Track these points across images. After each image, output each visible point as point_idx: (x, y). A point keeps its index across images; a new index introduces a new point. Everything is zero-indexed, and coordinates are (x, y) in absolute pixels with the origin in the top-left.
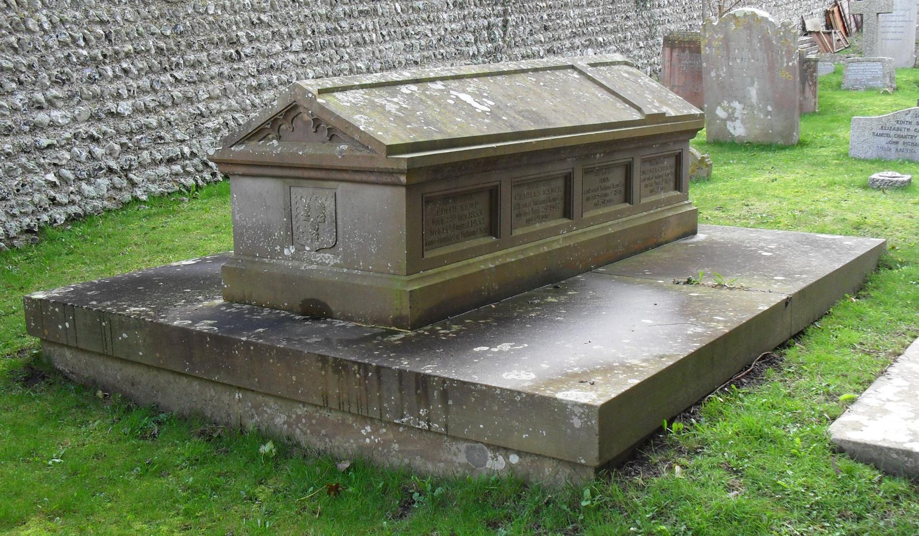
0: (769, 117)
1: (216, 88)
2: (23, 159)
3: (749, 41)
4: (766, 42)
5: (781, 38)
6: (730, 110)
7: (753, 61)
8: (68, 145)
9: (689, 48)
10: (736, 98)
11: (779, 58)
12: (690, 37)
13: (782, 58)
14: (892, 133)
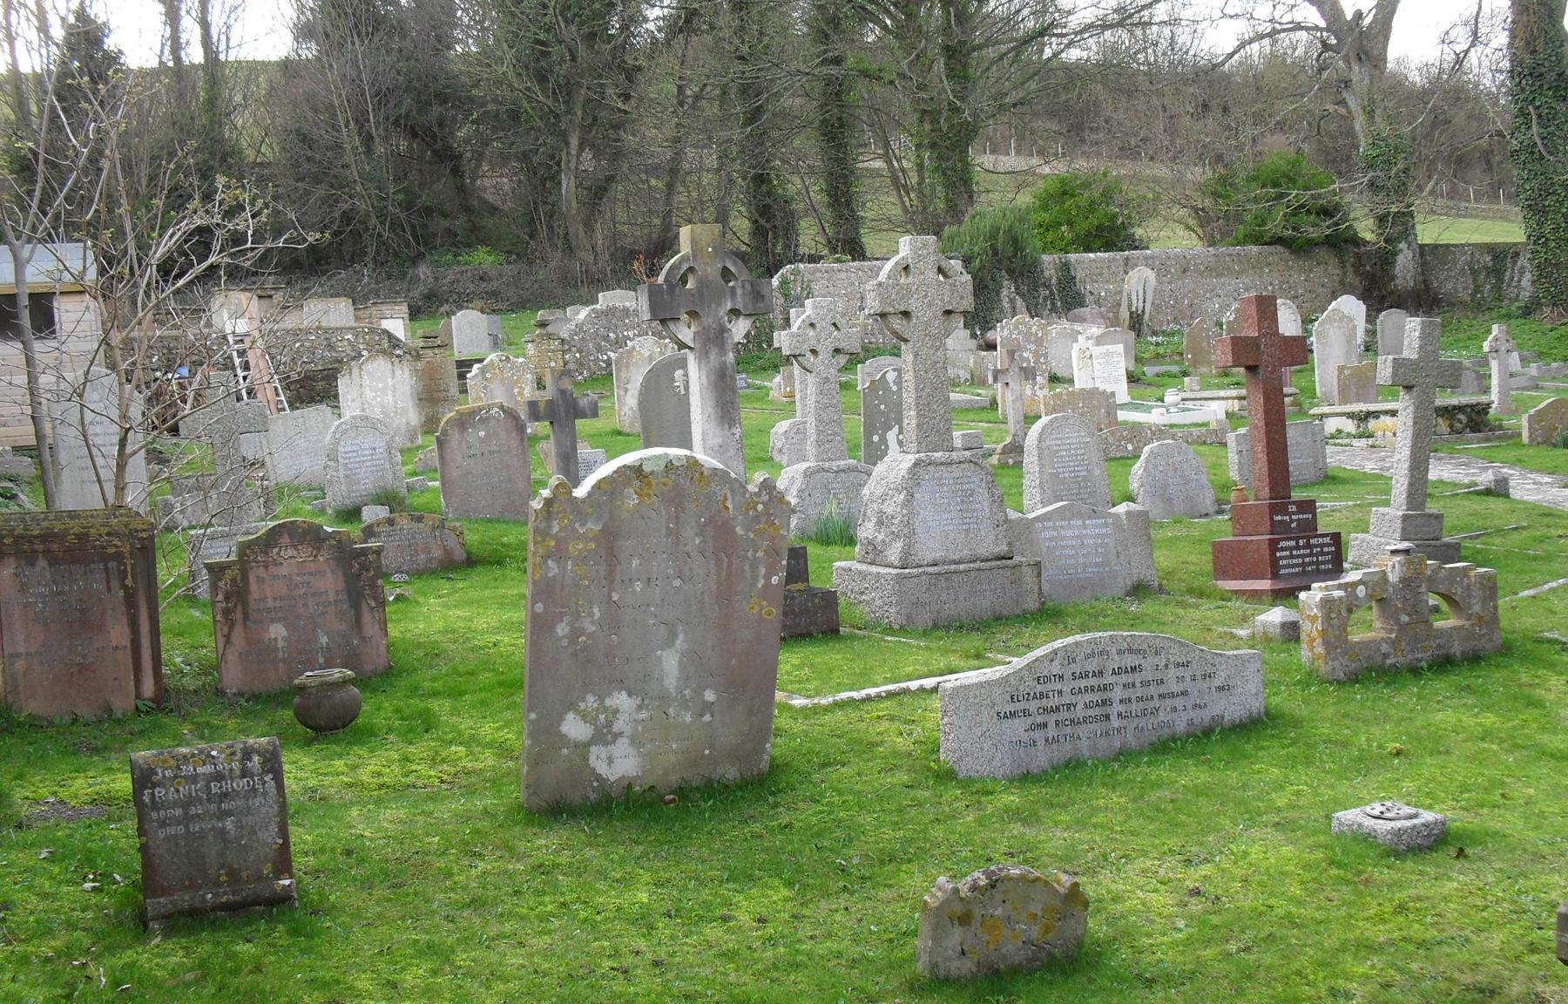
0: (707, 718)
3: (674, 534)
4: (721, 535)
5: (757, 518)
6: (602, 717)
7: (677, 583)
9: (48, 552)
10: (621, 684)
11: (747, 568)
12: (44, 524)
13: (754, 568)
14: (1033, 706)
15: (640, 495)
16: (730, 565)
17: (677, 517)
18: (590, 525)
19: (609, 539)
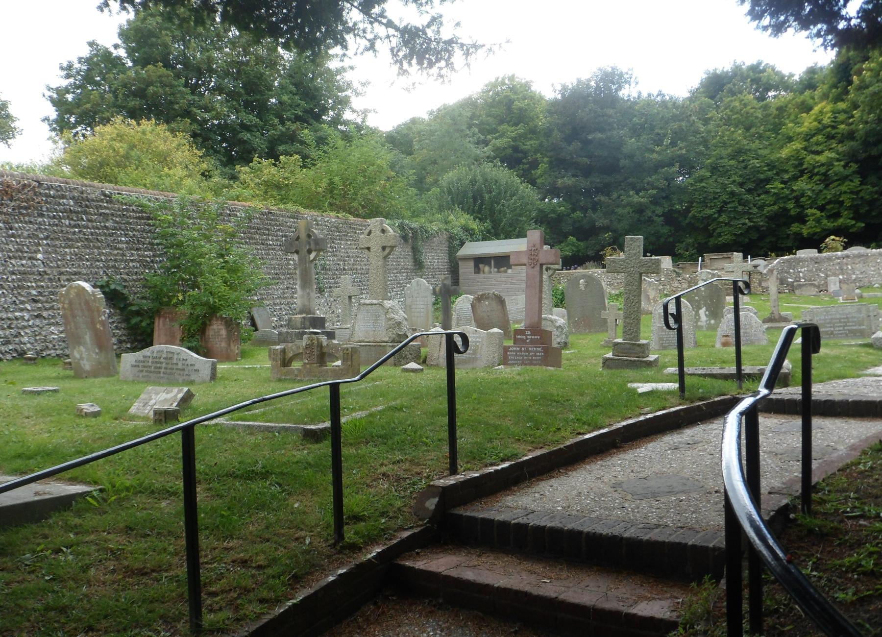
14: (141, 364)
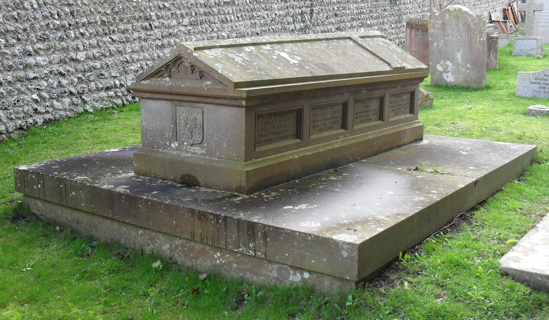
0: (468, 71)
1: (136, 46)
2: (19, 85)
3: (457, 25)
4: (468, 26)
7: (459, 37)
8: (46, 77)
9: (422, 29)
10: (448, 59)
11: (475, 36)
12: (422, 22)
13: (476, 36)
14: (542, 82)
15: (449, 16)
16: (470, 35)
17: (458, 22)
18: (439, 21)
19: (444, 25)
